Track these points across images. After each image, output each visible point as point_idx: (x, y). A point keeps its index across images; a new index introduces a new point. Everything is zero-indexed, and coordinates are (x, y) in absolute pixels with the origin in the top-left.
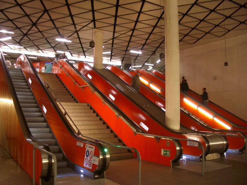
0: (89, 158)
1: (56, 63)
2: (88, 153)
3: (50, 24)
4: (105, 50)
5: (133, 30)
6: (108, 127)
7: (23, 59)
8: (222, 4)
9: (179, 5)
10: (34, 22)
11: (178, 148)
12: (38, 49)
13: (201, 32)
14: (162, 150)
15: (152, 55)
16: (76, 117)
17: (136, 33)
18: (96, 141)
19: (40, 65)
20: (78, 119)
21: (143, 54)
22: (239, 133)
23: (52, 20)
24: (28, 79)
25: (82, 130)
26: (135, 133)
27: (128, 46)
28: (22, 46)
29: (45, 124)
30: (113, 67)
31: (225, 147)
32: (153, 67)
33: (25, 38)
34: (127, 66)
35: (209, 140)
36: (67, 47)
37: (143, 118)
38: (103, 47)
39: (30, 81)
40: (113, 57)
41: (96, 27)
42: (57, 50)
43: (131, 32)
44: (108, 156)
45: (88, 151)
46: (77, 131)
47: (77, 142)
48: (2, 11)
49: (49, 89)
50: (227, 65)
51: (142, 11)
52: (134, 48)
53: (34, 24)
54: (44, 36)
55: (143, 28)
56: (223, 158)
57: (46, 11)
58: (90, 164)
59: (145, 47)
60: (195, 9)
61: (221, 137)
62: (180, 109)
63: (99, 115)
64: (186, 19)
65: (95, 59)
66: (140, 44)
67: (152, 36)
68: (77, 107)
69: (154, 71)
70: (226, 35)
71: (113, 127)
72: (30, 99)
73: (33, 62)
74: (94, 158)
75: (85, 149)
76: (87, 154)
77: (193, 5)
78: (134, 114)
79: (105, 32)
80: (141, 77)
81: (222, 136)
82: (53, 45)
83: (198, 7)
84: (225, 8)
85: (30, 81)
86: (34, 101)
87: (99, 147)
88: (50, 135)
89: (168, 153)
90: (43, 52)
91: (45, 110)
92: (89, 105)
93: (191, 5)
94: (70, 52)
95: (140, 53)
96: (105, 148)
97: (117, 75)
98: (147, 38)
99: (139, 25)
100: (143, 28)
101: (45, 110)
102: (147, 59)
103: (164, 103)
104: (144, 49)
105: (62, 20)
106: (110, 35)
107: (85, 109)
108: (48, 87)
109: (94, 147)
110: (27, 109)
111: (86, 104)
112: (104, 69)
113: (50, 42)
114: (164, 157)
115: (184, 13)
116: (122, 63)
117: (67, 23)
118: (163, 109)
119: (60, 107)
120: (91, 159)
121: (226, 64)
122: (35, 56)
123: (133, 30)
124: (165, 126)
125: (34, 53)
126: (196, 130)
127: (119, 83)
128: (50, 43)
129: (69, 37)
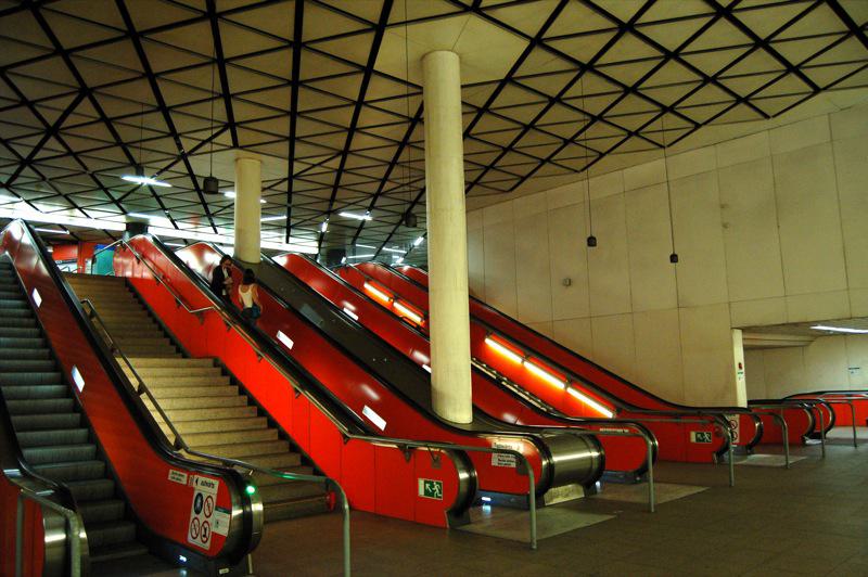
0: (202, 517)
1: (124, 247)
2: (199, 501)
3: (101, 131)
4: (266, 211)
5: (345, 153)
6: (272, 424)
7: (17, 235)
8: (578, 82)
9: (467, 83)
10: (52, 122)
11: (463, 475)
12: (70, 205)
13: (530, 160)
14: (421, 482)
15: (399, 224)
16: (174, 400)
17: (351, 162)
18: (226, 463)
19: (80, 252)
20: (190, 415)
21: (374, 220)
22: (634, 426)
23: (108, 122)
24: (32, 291)
25: (185, 435)
26: (345, 436)
27: (332, 199)
28: (19, 197)
29: (82, 432)
30: (292, 257)
31: (595, 466)
32: (405, 256)
33: (27, 171)
34: (333, 255)
35: (551, 449)
36: (158, 202)
37: (373, 395)
38: (263, 201)
39: (37, 298)
40: (293, 232)
41: (241, 143)
42: (131, 211)
43: (339, 159)
44: (257, 507)
45: (200, 495)
46: (172, 440)
47: (171, 471)
48: (5, 142)
49: (94, 320)
50: (595, 245)
51: (366, 99)
52: (350, 204)
53: (53, 131)
54: (86, 168)
55: (371, 148)
56: (594, 496)
57: (85, 92)
58: (205, 536)
59: (380, 201)
60: (510, 95)
61: (583, 440)
62: (473, 367)
63: (287, 435)
64: (486, 123)
65: (240, 234)
66: (362, 195)
67: (396, 172)
68: (181, 371)
69: (406, 268)
70: (590, 169)
71: (285, 424)
72: (20, 316)
73: (49, 240)
74: (217, 515)
75: (193, 489)
76: (198, 505)
77: (502, 84)
78: (350, 385)
79: (264, 158)
80: (399, 303)
81: (585, 435)
82: (117, 196)
83: (317, 56)
84: (584, 94)
85: (37, 298)
86: (99, 466)
87: (232, 481)
88: (99, 466)
89: (436, 487)
90: (88, 216)
91: (80, 382)
92: (219, 362)
93: (496, 86)
94: (169, 216)
95: (368, 218)
96: (249, 483)
97: (302, 279)
98: (382, 176)
99: (360, 141)
100: (371, 148)
101: (80, 382)
102: (391, 239)
103: (427, 352)
104: (376, 208)
105: (136, 121)
106: (280, 169)
107: (205, 376)
108: (93, 314)
109: (216, 483)
110: (36, 417)
111: (210, 362)
112: (265, 261)
113: (106, 185)
114: (427, 503)
115: (481, 104)
116: (320, 247)
117: (149, 129)
118: (425, 367)
119: (127, 371)
120: (209, 520)
121: (591, 241)
122: (62, 227)
123: (345, 153)
124: (429, 414)
125: (54, 214)
126: (519, 423)
127: (310, 305)
128: (106, 190)
129: (162, 171)
